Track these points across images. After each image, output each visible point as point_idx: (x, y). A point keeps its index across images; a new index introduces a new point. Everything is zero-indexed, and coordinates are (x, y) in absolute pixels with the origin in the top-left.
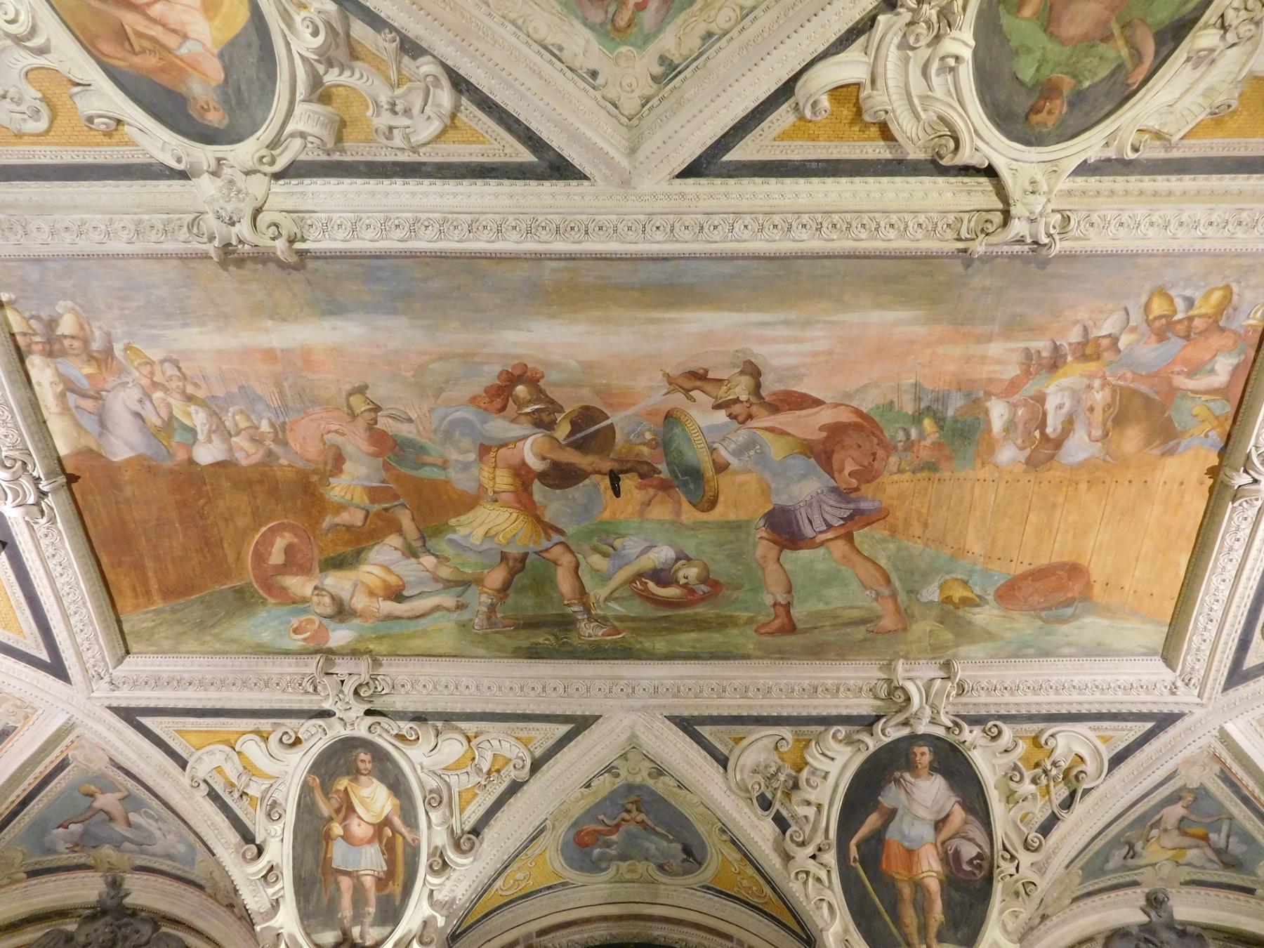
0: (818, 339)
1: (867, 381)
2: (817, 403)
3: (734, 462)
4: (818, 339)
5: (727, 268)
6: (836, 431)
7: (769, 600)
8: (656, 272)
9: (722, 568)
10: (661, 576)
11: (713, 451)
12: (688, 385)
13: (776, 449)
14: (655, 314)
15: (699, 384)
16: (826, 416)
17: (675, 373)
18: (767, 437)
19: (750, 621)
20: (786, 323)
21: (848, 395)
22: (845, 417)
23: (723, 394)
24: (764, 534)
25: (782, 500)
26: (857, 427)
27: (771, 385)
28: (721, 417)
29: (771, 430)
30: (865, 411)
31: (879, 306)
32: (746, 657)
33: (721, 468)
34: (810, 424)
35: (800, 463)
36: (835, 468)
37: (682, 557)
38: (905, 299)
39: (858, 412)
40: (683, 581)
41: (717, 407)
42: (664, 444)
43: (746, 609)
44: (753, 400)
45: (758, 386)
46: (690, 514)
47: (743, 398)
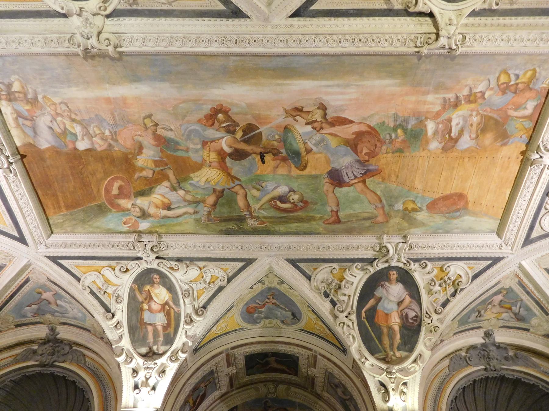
0: (352, 93)
1: (373, 112)
2: (351, 122)
3: (315, 149)
4: (352, 93)
5: (311, 60)
6: (359, 135)
7: (329, 209)
8: (280, 62)
9: (309, 195)
10: (283, 199)
11: (305, 143)
12: (294, 114)
13: (333, 143)
14: (280, 82)
15: (299, 113)
16: (355, 128)
17: (288, 108)
18: (329, 137)
19: (321, 218)
20: (338, 85)
21: (364, 119)
22: (364, 128)
23: (310, 118)
24: (327, 181)
25: (335, 165)
26: (368, 133)
27: (331, 114)
28: (309, 128)
29: (331, 134)
30: (372, 126)
31: (379, 78)
32: (319, 234)
33: (309, 151)
34: (348, 132)
35: (343, 149)
36: (359, 151)
37: (292, 191)
38: (391, 75)
39: (369, 126)
40: (292, 201)
41: (307, 124)
42: (284, 141)
43: (319, 213)
44: (323, 120)
45: (325, 114)
46: (295, 172)
47: (319, 120)
